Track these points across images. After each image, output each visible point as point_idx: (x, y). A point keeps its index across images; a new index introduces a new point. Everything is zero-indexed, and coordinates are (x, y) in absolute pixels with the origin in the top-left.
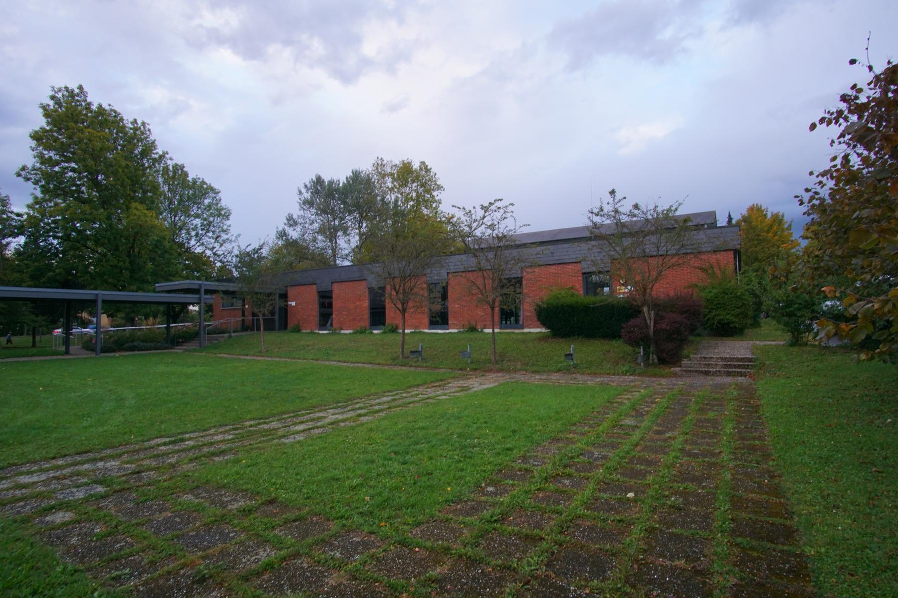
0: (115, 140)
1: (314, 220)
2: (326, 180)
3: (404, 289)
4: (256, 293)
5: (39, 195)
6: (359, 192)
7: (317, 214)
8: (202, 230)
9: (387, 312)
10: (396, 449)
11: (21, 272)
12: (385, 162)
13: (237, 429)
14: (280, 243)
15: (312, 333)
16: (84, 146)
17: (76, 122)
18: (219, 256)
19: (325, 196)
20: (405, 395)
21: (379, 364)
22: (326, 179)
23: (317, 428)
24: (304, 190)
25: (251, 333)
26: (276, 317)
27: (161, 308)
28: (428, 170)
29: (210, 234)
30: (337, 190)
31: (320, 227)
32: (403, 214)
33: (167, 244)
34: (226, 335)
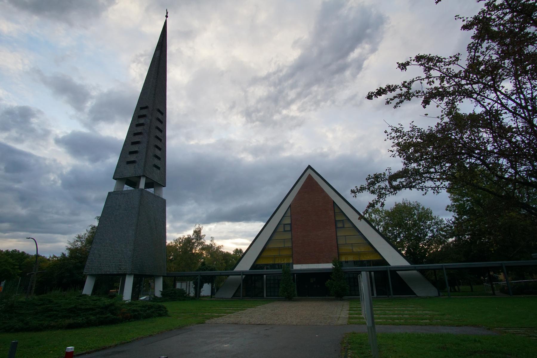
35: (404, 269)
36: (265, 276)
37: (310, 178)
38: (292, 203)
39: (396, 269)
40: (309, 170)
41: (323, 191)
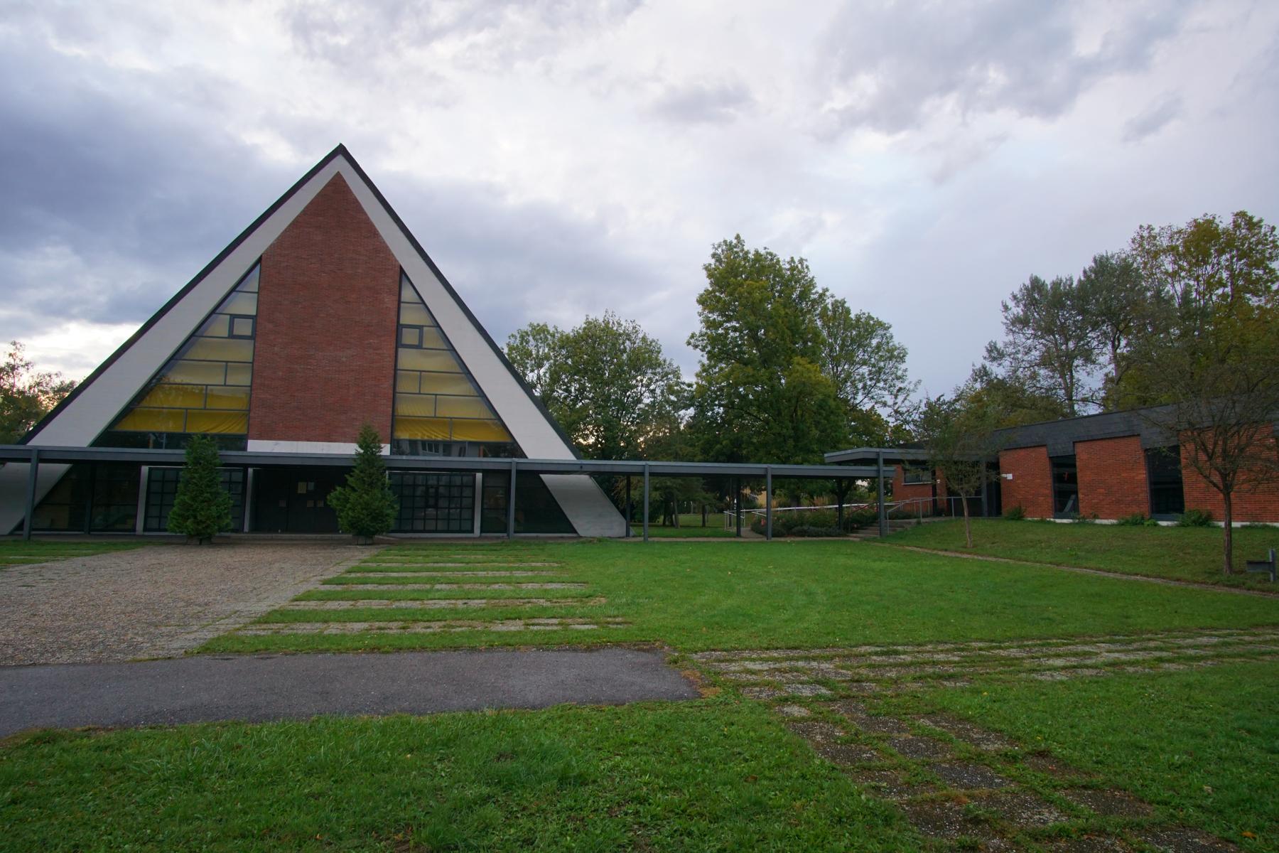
0: (773, 286)
1: (1032, 346)
2: (1048, 282)
3: (1224, 451)
4: (956, 463)
5: (706, 362)
6: (1110, 290)
7: (1035, 336)
8: (871, 379)
9: (1185, 489)
10: (1250, 725)
11: (693, 446)
12: (1157, 230)
13: (963, 650)
14: (978, 386)
15: (1043, 521)
16: (744, 302)
17: (736, 276)
18: (902, 414)
19: (1046, 307)
20: (1247, 638)
21: (1178, 580)
22: (1048, 279)
23: (1087, 667)
24: (1011, 304)
25: (948, 518)
26: (984, 497)
27: (829, 485)
28: (1252, 225)
29: (881, 384)
30: (1067, 294)
31: (1042, 357)
32: (1203, 314)
33: (832, 403)
34: (914, 520)
35: (562, 469)
36: (145, 469)
37: (338, 183)
38: (266, 252)
39: (539, 468)
40: (340, 160)
41: (373, 232)
